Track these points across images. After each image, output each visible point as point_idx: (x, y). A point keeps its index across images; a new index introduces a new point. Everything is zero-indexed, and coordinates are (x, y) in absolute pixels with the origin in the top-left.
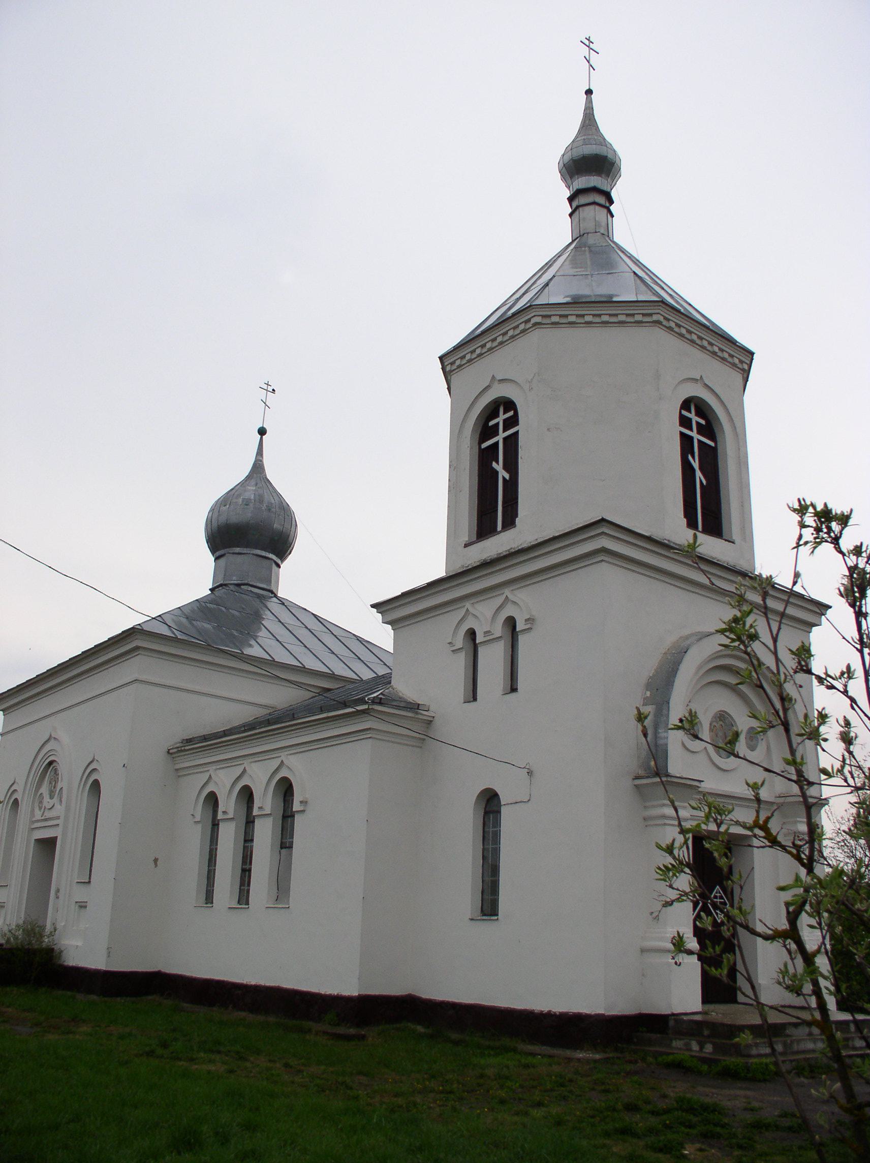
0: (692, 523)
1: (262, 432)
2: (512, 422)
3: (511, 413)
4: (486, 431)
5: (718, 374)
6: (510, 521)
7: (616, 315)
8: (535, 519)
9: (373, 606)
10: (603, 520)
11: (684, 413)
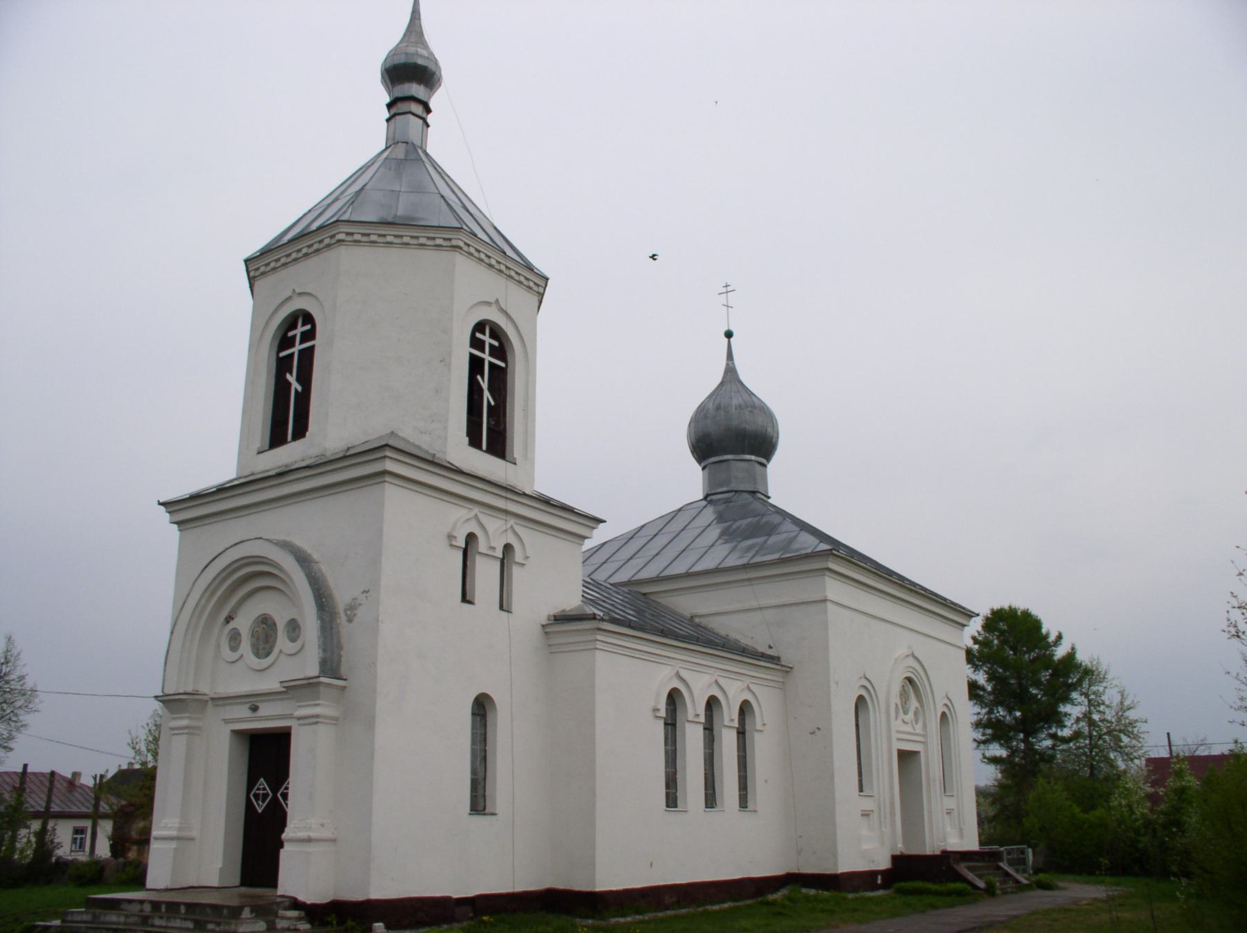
0: (475, 441)
1: (729, 335)
2: (309, 335)
3: (308, 327)
4: (285, 342)
5: (516, 298)
6: (301, 431)
7: (417, 238)
8: (334, 425)
11: (478, 335)
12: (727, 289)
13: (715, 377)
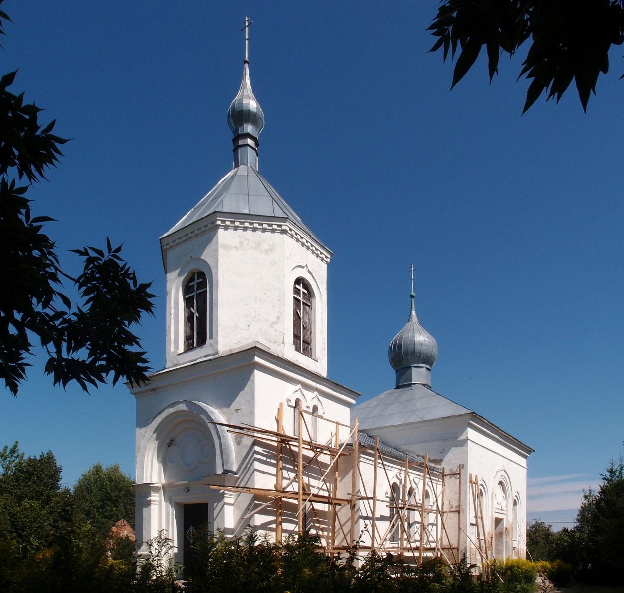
0: (297, 349)
6: (202, 341)
11: (297, 286)
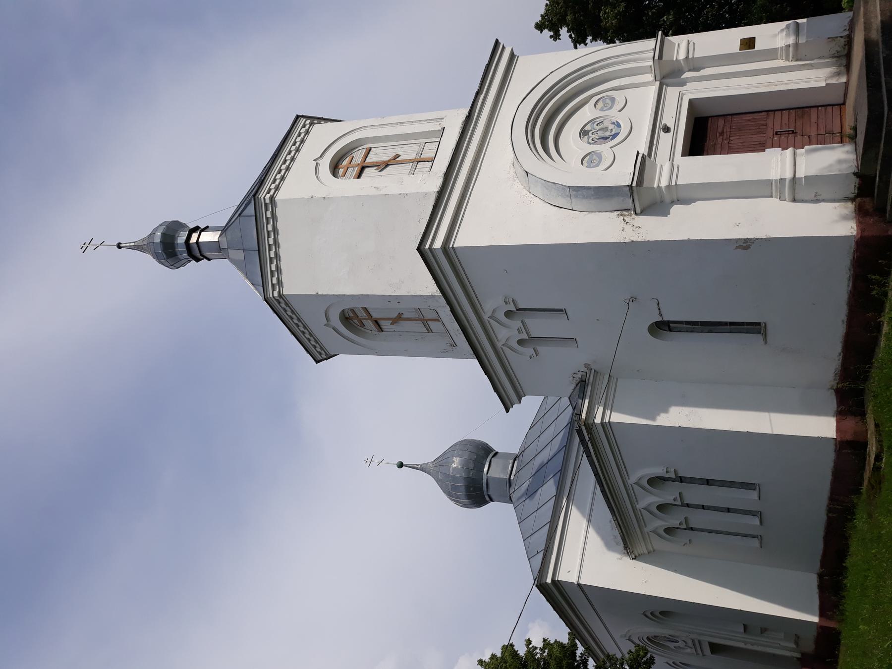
1: (401, 465)
9: (507, 411)
10: (420, 249)
12: (369, 462)
13: (429, 483)
